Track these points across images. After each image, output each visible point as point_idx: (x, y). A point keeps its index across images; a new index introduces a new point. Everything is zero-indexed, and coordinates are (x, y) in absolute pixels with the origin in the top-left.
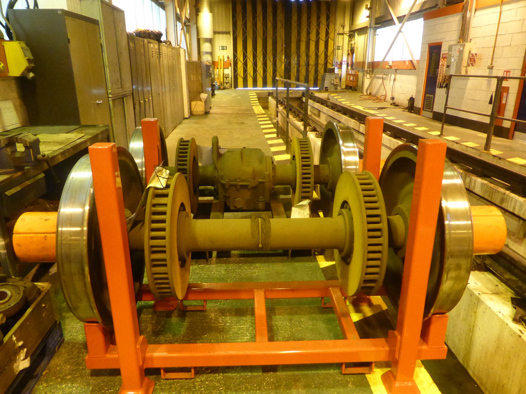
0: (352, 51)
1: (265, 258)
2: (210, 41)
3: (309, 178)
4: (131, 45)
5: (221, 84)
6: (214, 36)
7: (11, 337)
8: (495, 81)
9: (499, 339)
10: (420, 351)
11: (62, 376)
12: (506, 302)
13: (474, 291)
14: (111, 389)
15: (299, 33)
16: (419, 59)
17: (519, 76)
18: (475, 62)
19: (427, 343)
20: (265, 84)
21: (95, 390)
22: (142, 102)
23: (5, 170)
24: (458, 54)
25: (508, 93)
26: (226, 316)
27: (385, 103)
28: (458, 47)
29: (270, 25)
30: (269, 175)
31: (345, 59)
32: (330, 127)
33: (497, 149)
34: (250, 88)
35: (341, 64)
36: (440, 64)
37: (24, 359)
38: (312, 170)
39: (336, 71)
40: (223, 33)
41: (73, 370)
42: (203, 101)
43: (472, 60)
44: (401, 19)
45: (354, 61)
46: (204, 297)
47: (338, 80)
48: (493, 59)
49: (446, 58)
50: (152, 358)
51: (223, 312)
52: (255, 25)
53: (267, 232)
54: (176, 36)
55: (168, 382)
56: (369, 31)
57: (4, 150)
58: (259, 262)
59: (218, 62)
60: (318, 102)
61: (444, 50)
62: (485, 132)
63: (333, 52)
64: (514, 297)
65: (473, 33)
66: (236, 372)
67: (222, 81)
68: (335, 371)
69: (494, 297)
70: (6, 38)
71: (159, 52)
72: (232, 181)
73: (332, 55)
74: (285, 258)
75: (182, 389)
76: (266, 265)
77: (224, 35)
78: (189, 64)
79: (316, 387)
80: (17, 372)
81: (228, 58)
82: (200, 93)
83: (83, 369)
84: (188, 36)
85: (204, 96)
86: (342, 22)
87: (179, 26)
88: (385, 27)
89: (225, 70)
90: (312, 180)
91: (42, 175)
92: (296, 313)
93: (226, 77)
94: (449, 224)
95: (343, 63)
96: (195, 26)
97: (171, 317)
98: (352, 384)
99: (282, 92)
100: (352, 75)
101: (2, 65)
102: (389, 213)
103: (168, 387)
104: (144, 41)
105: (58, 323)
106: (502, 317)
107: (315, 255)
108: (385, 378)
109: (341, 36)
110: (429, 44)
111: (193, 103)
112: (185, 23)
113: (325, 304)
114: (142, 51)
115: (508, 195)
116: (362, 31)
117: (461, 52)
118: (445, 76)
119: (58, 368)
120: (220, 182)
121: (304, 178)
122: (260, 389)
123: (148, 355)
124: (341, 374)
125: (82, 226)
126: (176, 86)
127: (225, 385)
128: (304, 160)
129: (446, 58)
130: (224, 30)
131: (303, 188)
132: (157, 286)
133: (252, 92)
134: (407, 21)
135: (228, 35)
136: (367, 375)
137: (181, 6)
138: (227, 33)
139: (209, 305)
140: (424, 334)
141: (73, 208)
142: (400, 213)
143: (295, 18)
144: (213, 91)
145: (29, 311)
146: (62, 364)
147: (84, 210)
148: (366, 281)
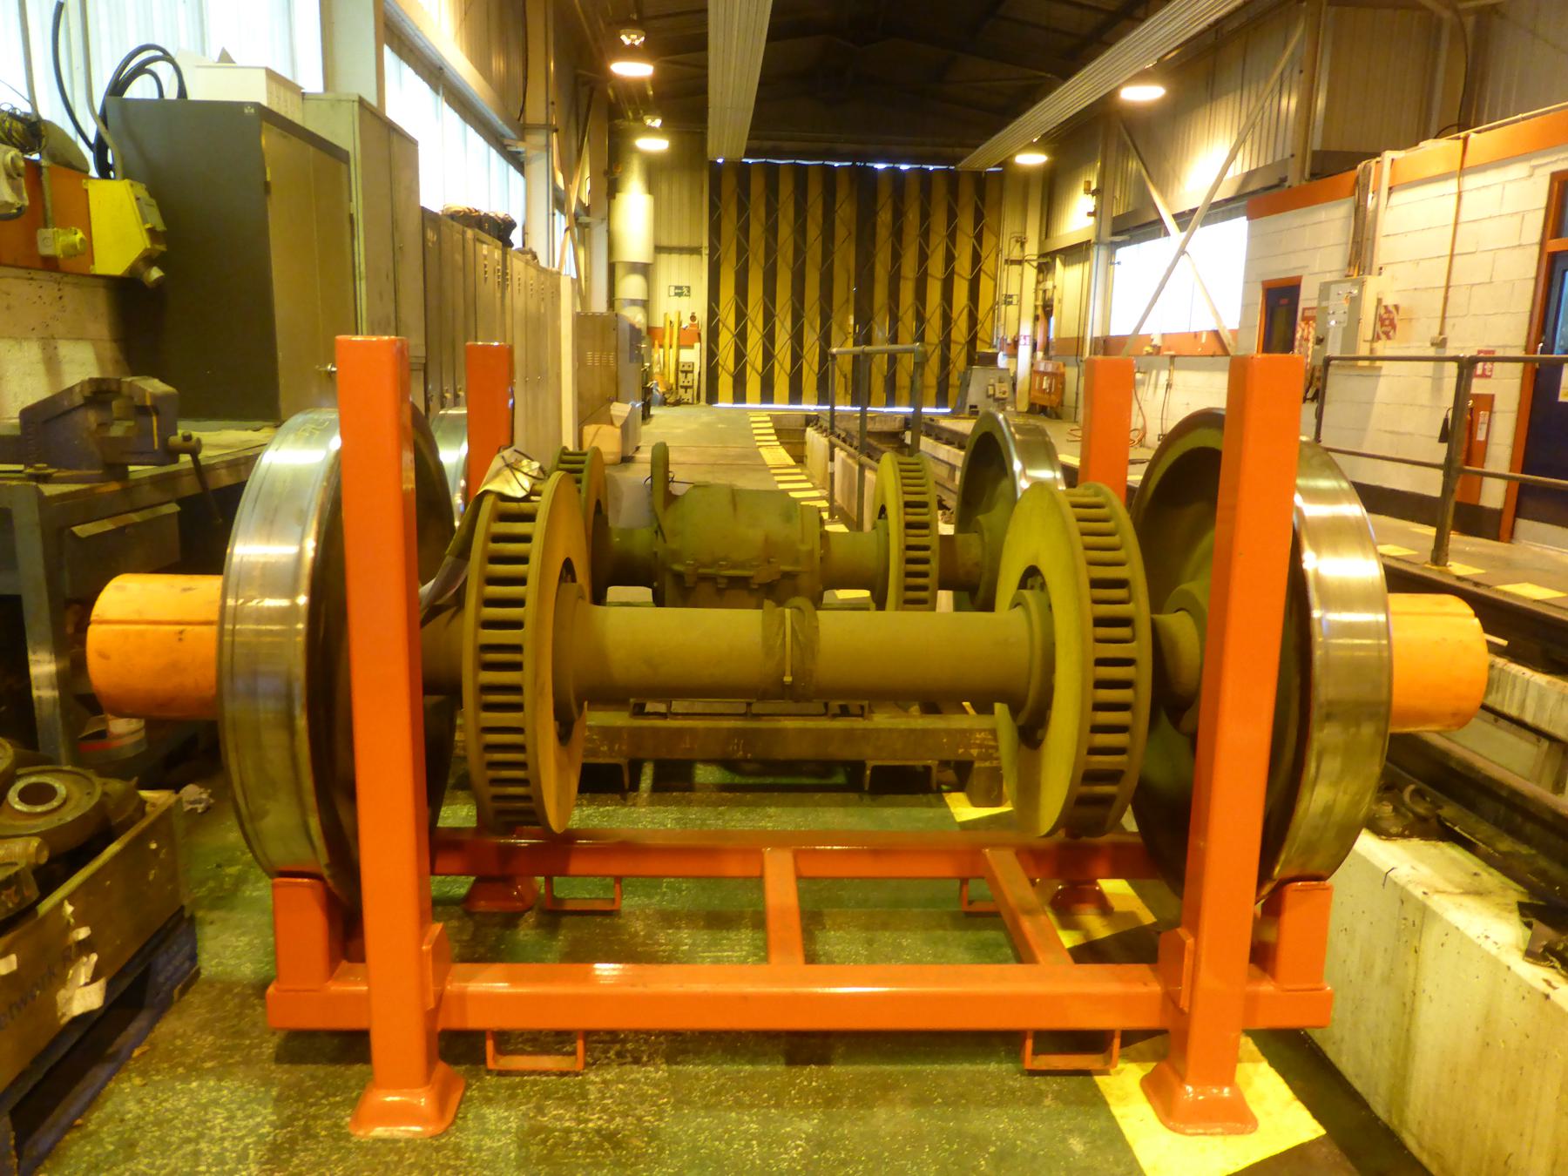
0: (1046, 309)
1: (792, 795)
2: (645, 270)
3: (926, 561)
4: (430, 235)
5: (670, 390)
6: (655, 258)
7: (60, 905)
8: (1452, 369)
9: (1488, 1018)
10: (1252, 1001)
11: (189, 1061)
12: (1506, 914)
13: (1410, 887)
14: (335, 1095)
15: (896, 257)
16: (1236, 327)
17: (1520, 353)
18: (1394, 327)
19: (1273, 976)
20: (796, 395)
21: (289, 1097)
22: (448, 395)
23: (74, 473)
24: (1346, 305)
25: (1491, 412)
26: (679, 928)
27: (1142, 450)
28: (1345, 289)
29: (814, 232)
30: (811, 553)
31: (1026, 329)
32: (986, 429)
33: (1466, 563)
34: (753, 403)
35: (1016, 343)
36: (1298, 336)
37: (86, 984)
38: (934, 557)
39: (1002, 361)
40: (681, 250)
41: (224, 1048)
42: (618, 423)
43: (1387, 322)
44: (1183, 219)
45: (1052, 336)
46: (617, 866)
47: (1006, 387)
48: (1444, 318)
49: (1313, 318)
50: (462, 997)
51: (669, 919)
52: (772, 230)
53: (807, 644)
54: (549, 240)
55: (506, 1081)
56: (1093, 253)
57: (78, 416)
58: (777, 805)
59: (663, 330)
60: (948, 443)
61: (1308, 297)
62: (1431, 525)
63: (993, 309)
64: (1526, 900)
65: (1384, 250)
66: (706, 1063)
67: (672, 380)
68: (1004, 1067)
69: (1468, 901)
70: (93, 172)
71: (505, 273)
72: (705, 566)
73: (993, 256)
74: (853, 796)
75: (547, 1098)
76: (799, 811)
77: (686, 257)
78: (583, 321)
79: (946, 1103)
80: (65, 1020)
81: (693, 318)
82: (611, 401)
83: (251, 1047)
84: (581, 253)
85: (620, 410)
86: (1018, 229)
87: (561, 222)
88: (1139, 242)
89: (683, 352)
90: (933, 567)
91: (173, 508)
92: (885, 926)
93: (683, 370)
94: (1320, 620)
95: (1022, 342)
96: (604, 226)
97: (516, 926)
98: (1056, 1098)
99: (848, 416)
100: (1045, 373)
101: (80, 235)
102: (1157, 606)
103: (504, 1093)
104: (464, 233)
105: (187, 914)
106: (1494, 951)
107: (940, 791)
108: (1155, 1088)
109: (1015, 269)
110: (1264, 283)
111: (589, 430)
112: (576, 216)
113: (971, 903)
114: (459, 258)
115: (1502, 670)
116: (1075, 253)
117: (1355, 302)
118: (1314, 369)
119: (179, 1042)
120: (671, 570)
121: (909, 561)
122: (777, 1106)
123: (452, 987)
124: (1022, 1074)
125: (292, 593)
126: (544, 377)
127: (674, 1092)
128: (910, 510)
129: (1313, 318)
130: (685, 243)
131: (908, 588)
132: (492, 774)
133: (758, 415)
134: (1202, 225)
135: (695, 257)
136: (1097, 1079)
137: (569, 170)
138: (694, 251)
139: (628, 903)
140: (1262, 956)
141: (271, 550)
142: (1188, 606)
143: (885, 217)
144: (646, 406)
145: (113, 848)
146: (190, 1033)
147: (300, 555)
148: (1091, 777)
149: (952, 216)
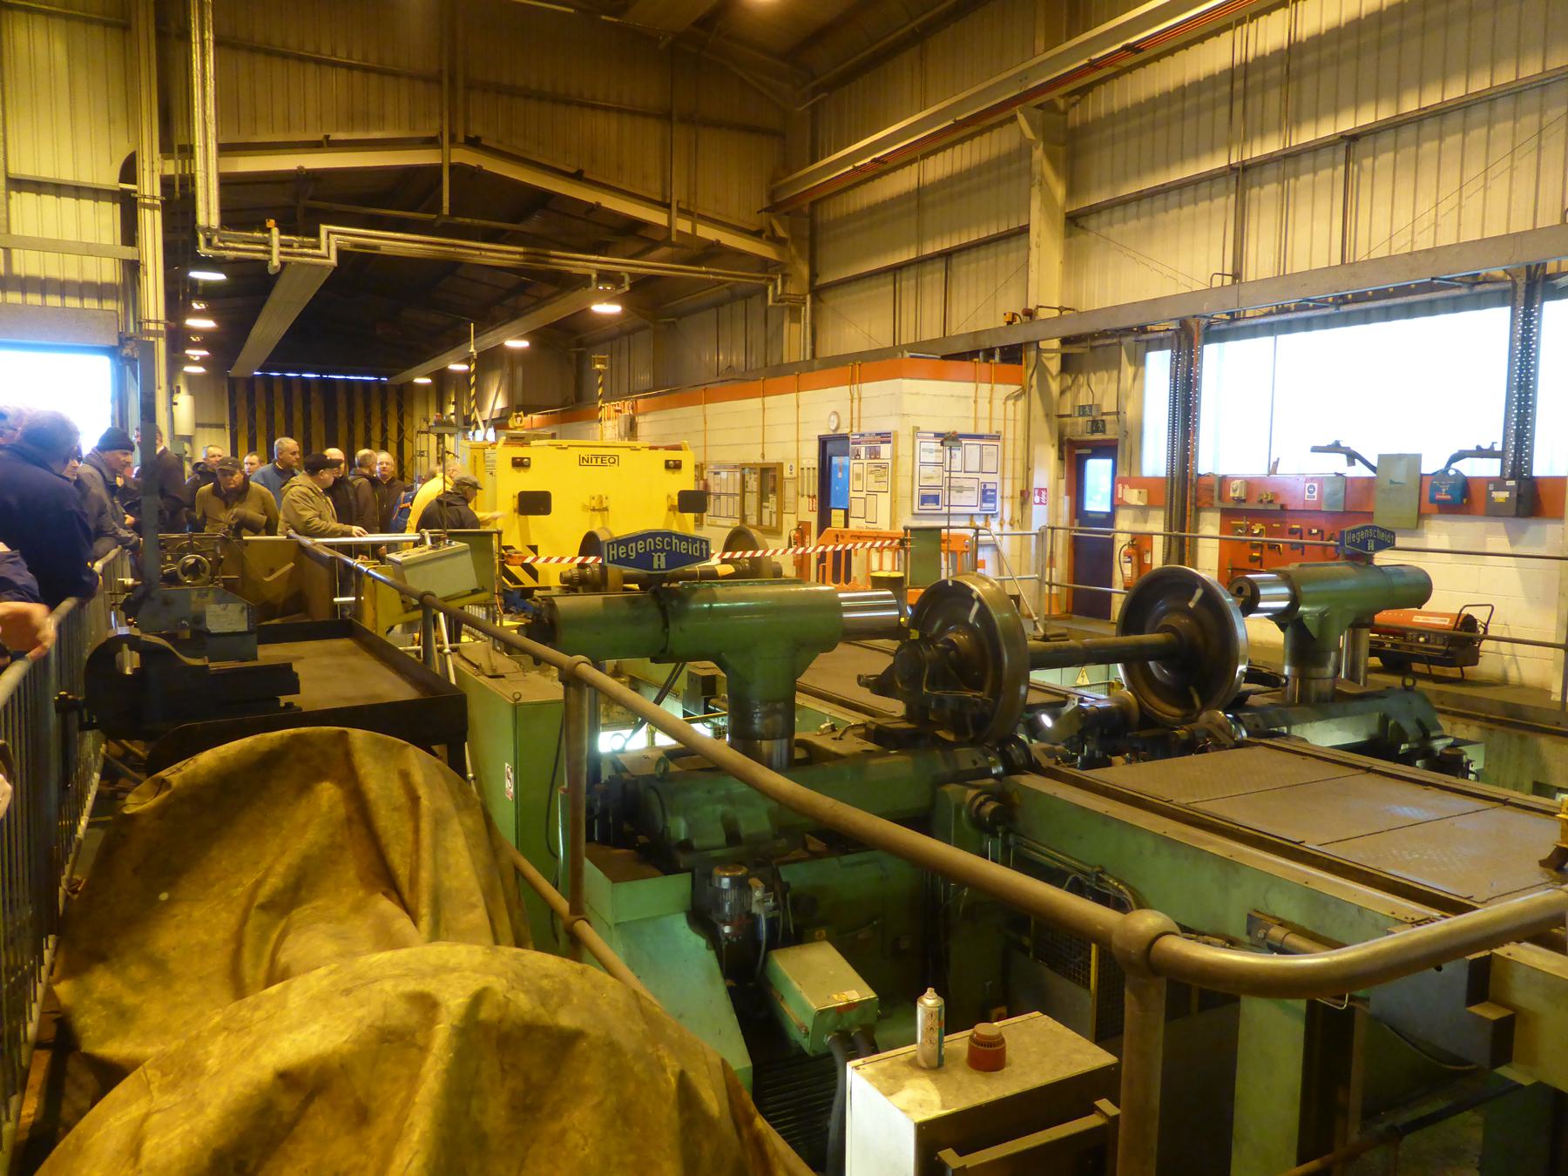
7: (50, 993)
40: (210, 426)
109: (424, 436)
130: (213, 421)
138: (222, 426)
149: (384, 407)
